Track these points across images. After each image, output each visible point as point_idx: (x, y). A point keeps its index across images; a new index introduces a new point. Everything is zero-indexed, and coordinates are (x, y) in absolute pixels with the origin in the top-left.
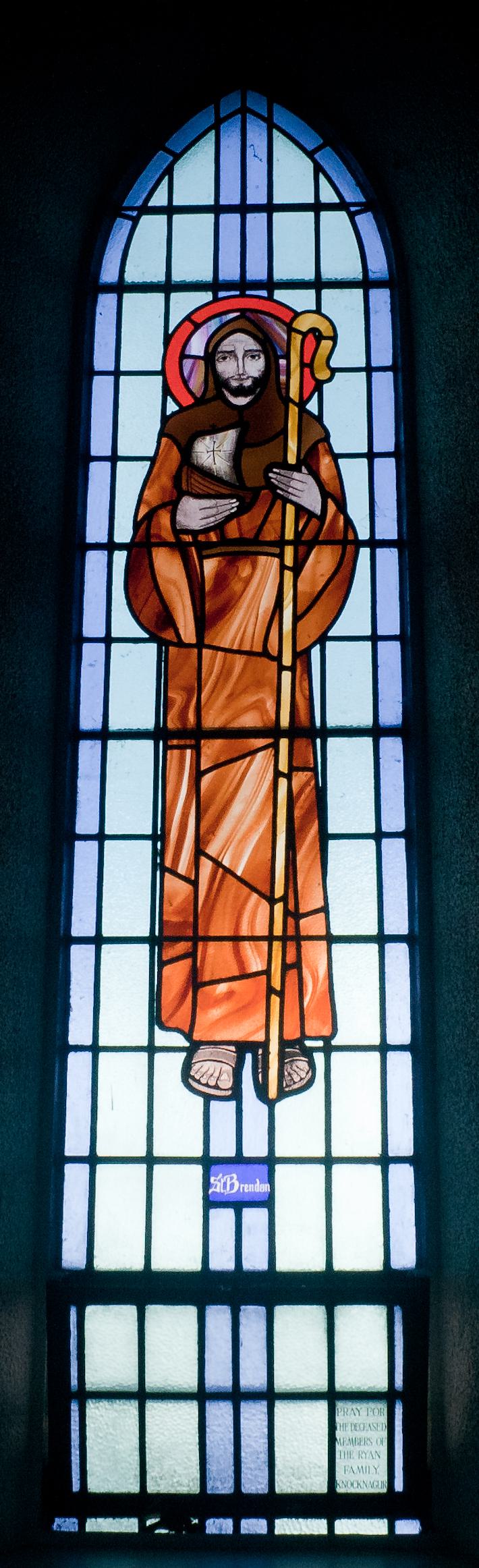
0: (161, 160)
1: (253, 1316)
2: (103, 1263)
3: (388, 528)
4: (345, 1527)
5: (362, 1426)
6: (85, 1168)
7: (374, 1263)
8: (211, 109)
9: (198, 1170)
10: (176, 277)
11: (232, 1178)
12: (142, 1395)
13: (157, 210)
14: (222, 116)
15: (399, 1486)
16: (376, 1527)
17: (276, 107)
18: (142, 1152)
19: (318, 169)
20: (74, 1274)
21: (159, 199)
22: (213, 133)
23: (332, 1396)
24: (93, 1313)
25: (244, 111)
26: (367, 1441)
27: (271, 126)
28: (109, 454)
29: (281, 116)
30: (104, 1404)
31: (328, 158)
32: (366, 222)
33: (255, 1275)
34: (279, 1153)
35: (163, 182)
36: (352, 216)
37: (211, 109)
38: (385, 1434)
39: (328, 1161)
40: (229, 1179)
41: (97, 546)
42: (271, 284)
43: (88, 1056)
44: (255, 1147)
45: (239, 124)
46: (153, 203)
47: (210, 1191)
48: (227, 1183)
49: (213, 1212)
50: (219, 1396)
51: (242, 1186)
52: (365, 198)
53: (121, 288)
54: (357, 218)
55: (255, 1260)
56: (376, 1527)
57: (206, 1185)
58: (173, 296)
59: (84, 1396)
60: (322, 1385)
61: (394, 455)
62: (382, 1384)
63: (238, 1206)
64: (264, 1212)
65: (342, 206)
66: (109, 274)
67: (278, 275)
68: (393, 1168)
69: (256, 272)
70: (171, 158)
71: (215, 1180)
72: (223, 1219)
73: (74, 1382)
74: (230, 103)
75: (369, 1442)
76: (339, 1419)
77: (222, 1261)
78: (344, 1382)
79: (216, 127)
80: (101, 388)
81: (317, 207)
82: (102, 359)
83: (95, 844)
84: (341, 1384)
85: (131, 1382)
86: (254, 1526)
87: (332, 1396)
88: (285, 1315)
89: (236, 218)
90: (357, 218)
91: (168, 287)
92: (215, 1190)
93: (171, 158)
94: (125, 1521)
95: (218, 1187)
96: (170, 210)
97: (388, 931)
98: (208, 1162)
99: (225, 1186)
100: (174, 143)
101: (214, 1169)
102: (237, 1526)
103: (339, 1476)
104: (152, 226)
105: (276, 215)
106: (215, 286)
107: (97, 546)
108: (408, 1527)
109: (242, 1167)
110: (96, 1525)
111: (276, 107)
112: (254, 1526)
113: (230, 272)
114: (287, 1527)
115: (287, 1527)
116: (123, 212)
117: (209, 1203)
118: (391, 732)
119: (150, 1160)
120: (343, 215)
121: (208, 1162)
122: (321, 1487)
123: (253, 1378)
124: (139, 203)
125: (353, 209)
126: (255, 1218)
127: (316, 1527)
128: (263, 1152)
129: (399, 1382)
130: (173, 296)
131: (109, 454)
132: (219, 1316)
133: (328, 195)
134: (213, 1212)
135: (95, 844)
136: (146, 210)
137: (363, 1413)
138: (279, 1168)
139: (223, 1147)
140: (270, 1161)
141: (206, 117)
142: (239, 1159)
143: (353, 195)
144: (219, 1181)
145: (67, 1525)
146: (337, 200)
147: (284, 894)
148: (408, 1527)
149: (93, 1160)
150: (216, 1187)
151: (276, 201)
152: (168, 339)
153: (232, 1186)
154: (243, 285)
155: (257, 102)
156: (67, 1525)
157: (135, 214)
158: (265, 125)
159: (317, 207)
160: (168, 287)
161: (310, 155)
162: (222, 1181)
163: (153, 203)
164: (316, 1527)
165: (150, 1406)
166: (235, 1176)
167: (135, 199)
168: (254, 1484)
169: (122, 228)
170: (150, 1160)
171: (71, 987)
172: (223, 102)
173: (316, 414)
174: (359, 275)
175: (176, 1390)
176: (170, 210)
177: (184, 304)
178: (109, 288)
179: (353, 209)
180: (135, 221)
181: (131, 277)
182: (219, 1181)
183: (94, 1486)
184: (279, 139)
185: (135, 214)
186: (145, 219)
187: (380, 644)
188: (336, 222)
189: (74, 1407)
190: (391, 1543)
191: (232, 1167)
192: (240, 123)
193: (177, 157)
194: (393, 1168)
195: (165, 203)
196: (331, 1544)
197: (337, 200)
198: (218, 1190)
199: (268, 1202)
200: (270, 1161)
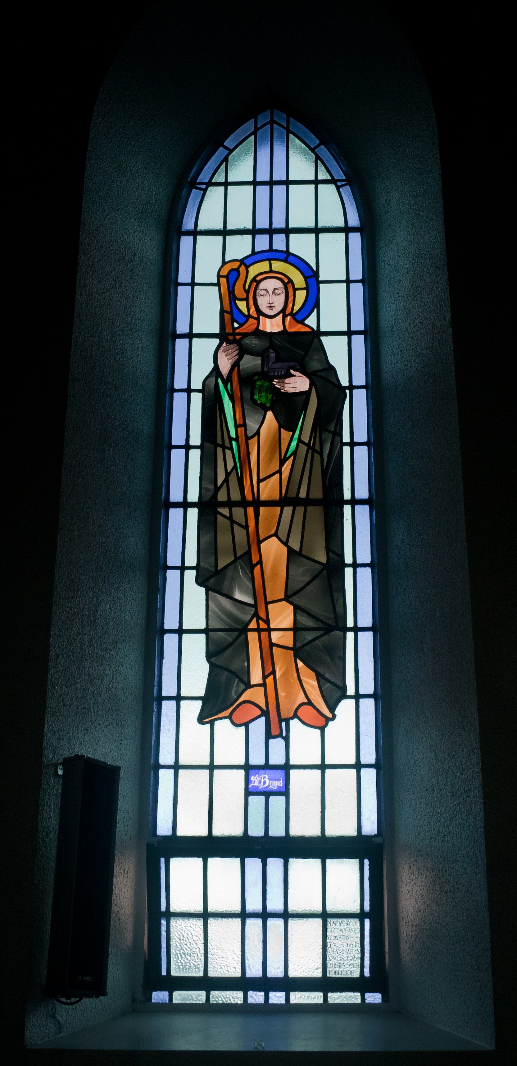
0: (220, 153)
1: (275, 865)
4: (335, 998)
6: (176, 636)
7: (351, 831)
9: (242, 772)
10: (229, 227)
11: (264, 778)
12: (205, 915)
15: (367, 973)
16: (354, 998)
17: (291, 119)
18: (216, 763)
19: (317, 158)
20: (165, 838)
21: (220, 178)
24: (175, 863)
25: (272, 122)
27: (289, 132)
28: (180, 565)
29: (295, 124)
30: (208, 776)
31: (323, 151)
32: (346, 191)
33: (277, 839)
36: (338, 188)
39: (212, 767)
40: (262, 778)
41: (182, 336)
43: (183, 451)
45: (269, 149)
47: (250, 786)
49: (251, 798)
51: (271, 782)
52: (213, 182)
53: (195, 233)
55: (277, 830)
56: (354, 998)
58: (228, 238)
59: (169, 915)
60: (318, 908)
61: (374, 696)
62: (355, 908)
63: (267, 794)
64: (283, 798)
65: (332, 181)
66: (188, 225)
68: (363, 771)
71: (253, 778)
72: (257, 802)
74: (263, 118)
77: (256, 830)
79: (255, 133)
80: (183, 293)
81: (316, 182)
82: (184, 276)
83: (189, 288)
84: (331, 908)
85: (200, 909)
86: (277, 998)
87: (325, 916)
88: (296, 864)
91: (224, 233)
92: (253, 785)
95: (256, 782)
96: (226, 184)
99: (260, 782)
100: (228, 143)
101: (251, 771)
107: (182, 336)
108: (374, 998)
110: (179, 997)
111: (291, 119)
112: (277, 998)
113: (263, 223)
116: (196, 186)
117: (248, 793)
119: (212, 767)
120: (332, 187)
121: (248, 768)
124: (207, 180)
125: (339, 184)
126: (277, 802)
127: (315, 998)
128: (282, 761)
129: (367, 907)
130: (228, 238)
131: (180, 565)
132: (254, 864)
133: (323, 175)
134: (251, 798)
135: (189, 288)
136: (211, 183)
138: (292, 772)
139: (257, 759)
140: (287, 767)
141: (249, 126)
142: (267, 766)
143: (339, 174)
144: (257, 779)
146: (329, 178)
147: (293, 606)
149: (176, 767)
150: (254, 783)
153: (265, 783)
154: (271, 231)
155: (281, 117)
156: (159, 996)
157: (204, 187)
158: (234, 519)
159: (316, 182)
160: (224, 233)
161: (313, 150)
162: (258, 779)
164: (315, 998)
165: (211, 921)
166: (267, 776)
167: (204, 177)
168: (276, 971)
170: (323, 767)
171: (159, 776)
172: (259, 117)
178: (188, 233)
179: (339, 184)
180: (205, 191)
181: (202, 226)
182: (257, 779)
185: (204, 187)
193: (231, 151)
194: (363, 771)
195: (223, 181)
197: (329, 178)
198: (256, 784)
199: (285, 792)
200: (287, 767)
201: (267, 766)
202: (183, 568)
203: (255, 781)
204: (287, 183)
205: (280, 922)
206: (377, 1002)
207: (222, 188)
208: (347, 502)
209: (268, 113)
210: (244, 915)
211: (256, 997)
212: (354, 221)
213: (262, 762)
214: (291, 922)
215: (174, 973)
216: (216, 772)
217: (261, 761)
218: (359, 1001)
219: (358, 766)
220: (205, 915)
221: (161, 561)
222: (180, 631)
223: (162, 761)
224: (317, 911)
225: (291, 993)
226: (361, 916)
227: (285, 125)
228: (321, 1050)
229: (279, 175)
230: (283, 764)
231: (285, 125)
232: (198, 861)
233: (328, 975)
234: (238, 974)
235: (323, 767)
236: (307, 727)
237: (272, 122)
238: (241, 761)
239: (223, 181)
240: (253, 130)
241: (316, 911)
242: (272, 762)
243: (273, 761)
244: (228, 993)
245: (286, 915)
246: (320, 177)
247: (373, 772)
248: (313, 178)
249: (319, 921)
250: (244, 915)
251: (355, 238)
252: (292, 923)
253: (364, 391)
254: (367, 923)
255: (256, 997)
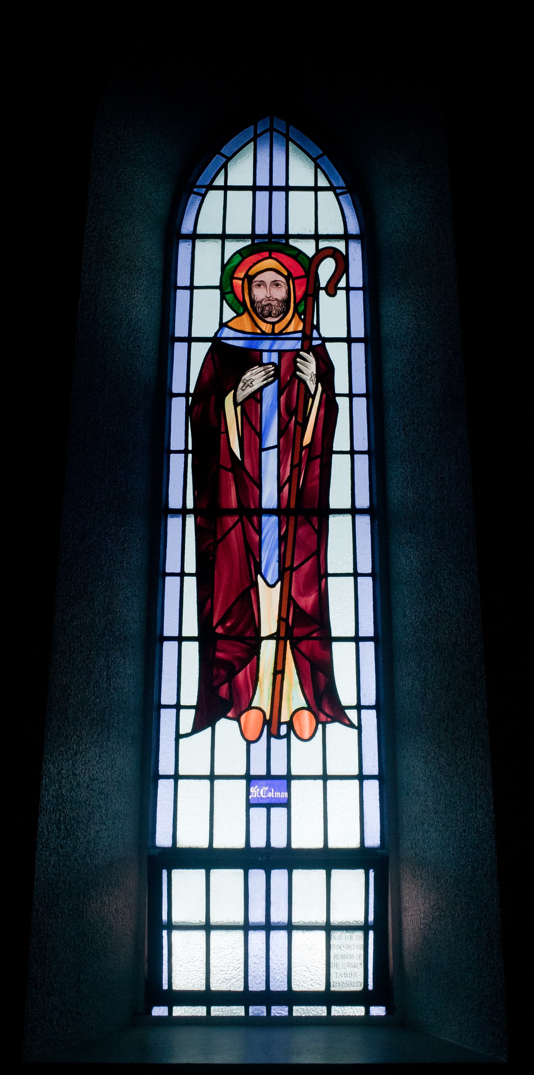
0: (218, 160)
2: (183, 842)
3: (169, 649)
4: (337, 1011)
5: (352, 946)
7: (354, 843)
8: (252, 127)
10: (228, 232)
12: (208, 927)
13: (218, 188)
14: (258, 133)
16: (359, 1011)
17: (291, 128)
18: (217, 773)
19: (317, 166)
20: (164, 850)
21: (219, 181)
22: (252, 143)
23: (328, 928)
24: (177, 874)
26: (351, 957)
27: (288, 139)
31: (325, 162)
33: (258, 850)
34: (294, 773)
35: (222, 172)
36: (337, 196)
37: (252, 127)
38: (362, 952)
41: (181, 340)
42: (287, 236)
44: (279, 769)
46: (216, 183)
47: (250, 797)
48: (258, 792)
50: (257, 927)
52: (345, 185)
53: (194, 237)
54: (340, 197)
55: (279, 842)
56: (359, 1011)
57: (248, 793)
63: (268, 806)
64: (284, 810)
65: (331, 188)
66: (187, 228)
67: (291, 232)
69: (278, 229)
70: (225, 160)
71: (253, 790)
72: (258, 814)
73: (165, 917)
74: (262, 125)
75: (352, 957)
76: (332, 942)
77: (258, 841)
78: (335, 919)
79: (254, 140)
81: (316, 189)
82: (183, 279)
83: (178, 579)
86: (279, 1011)
87: (328, 928)
89: (275, 183)
90: (340, 197)
91: (224, 237)
92: (253, 796)
93: (225, 160)
94: (221, 1014)
96: (226, 188)
97: (361, 634)
98: (249, 778)
101: (252, 782)
102: (269, 1011)
103: (333, 979)
104: (215, 197)
105: (193, 344)
106: (253, 236)
108: (378, 1011)
109: (270, 782)
110: (179, 1011)
111: (291, 128)
112: (279, 1011)
113: (262, 229)
114: (300, 1011)
115: (300, 1011)
117: (249, 805)
118: (362, 512)
120: (331, 194)
121: (249, 778)
122: (321, 987)
123: (257, 916)
125: (338, 191)
126: (278, 814)
128: (284, 772)
129: (371, 918)
132: (257, 876)
133: (323, 182)
135: (178, 579)
136: (211, 187)
137: (343, 938)
139: (258, 769)
140: (289, 777)
142: (268, 776)
145: (159, 1011)
148: (378, 1011)
149: (361, 777)
150: (254, 795)
151: (193, 335)
152: (223, 267)
155: (280, 124)
156: (159, 1011)
157: (203, 191)
160: (224, 237)
161: (314, 160)
163: (216, 183)
167: (203, 180)
168: (279, 985)
169: (194, 201)
170: (212, 777)
172: (259, 124)
173: (338, 286)
174: (341, 232)
175: (221, 924)
176: (226, 188)
177: (232, 247)
179: (338, 191)
180: (204, 196)
181: (201, 230)
182: (256, 790)
183: (177, 986)
184: (291, 146)
185: (203, 191)
186: (211, 194)
187: (356, 456)
188: (327, 198)
189: (165, 933)
190: (367, 1020)
191: (264, 782)
192: (269, 140)
193: (229, 159)
195: (223, 184)
196: (329, 1021)
199: (287, 804)
200: (289, 777)
201: (268, 776)
202: (182, 574)
203: (254, 793)
204: (287, 189)
205: (283, 934)
206: (165, 1015)
207: (222, 192)
208: (190, 511)
209: (268, 119)
210: (247, 927)
211: (258, 1011)
212: (354, 228)
213: (263, 772)
214: (214, 934)
215: (174, 988)
216: (180, 782)
217: (262, 771)
218: (243, 1014)
219: (361, 777)
220: (208, 927)
221: (161, 570)
222: (357, 639)
223: (166, 633)
224: (313, 923)
225: (272, 1007)
226: (365, 928)
227: (284, 132)
228: (364, 1063)
229: (279, 916)
230: (244, 774)
231: (284, 132)
232: (202, 873)
233: (272, 988)
234: (322, 988)
235: (212, 777)
236: (314, 738)
237: (271, 130)
238: (243, 772)
239: (223, 184)
240: (252, 136)
241: (347, 923)
242: (273, 773)
243: (275, 771)
244: (259, 1007)
245: (289, 927)
246: (320, 184)
247: (373, 713)
248: (312, 184)
249: (322, 934)
250: (247, 927)
251: (364, 522)
252: (214, 934)
253: (364, 400)
254: (371, 934)
255: (258, 1011)
